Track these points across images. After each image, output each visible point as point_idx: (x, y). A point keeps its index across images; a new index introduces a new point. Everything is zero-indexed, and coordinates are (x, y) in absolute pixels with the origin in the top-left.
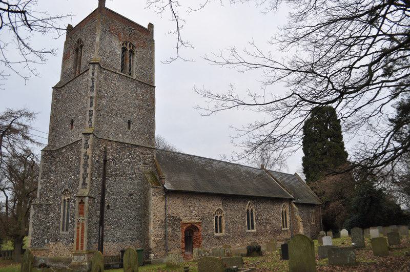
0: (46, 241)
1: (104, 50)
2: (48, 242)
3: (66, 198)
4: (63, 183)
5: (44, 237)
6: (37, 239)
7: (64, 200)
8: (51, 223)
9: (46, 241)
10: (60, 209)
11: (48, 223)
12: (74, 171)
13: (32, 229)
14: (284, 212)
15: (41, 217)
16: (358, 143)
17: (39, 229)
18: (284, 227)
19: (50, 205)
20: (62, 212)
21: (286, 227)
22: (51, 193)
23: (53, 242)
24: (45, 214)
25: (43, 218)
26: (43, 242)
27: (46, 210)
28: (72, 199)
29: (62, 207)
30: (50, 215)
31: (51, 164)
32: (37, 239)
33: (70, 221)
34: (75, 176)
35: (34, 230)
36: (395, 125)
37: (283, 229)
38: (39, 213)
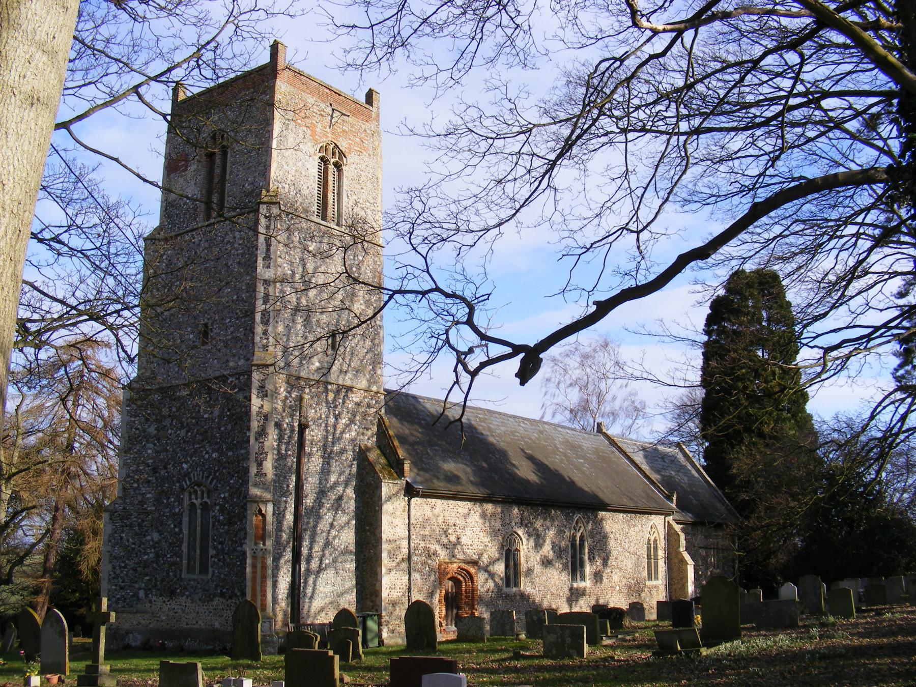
0: (142, 594)
1: (285, 167)
2: (147, 595)
3: (197, 502)
4: (185, 466)
5: (137, 586)
6: (122, 588)
7: (192, 505)
8: (151, 555)
9: (142, 594)
10: (180, 523)
11: (146, 554)
12: (217, 443)
13: (110, 567)
14: (652, 542)
15: (128, 541)
16: (844, 397)
17: (124, 567)
18: (650, 578)
19: (148, 514)
20: (186, 532)
21: (656, 578)
22: (148, 486)
23: (161, 595)
24: (136, 534)
25: (134, 544)
26: (136, 595)
27: (140, 525)
28: (216, 504)
29: (185, 519)
30: (149, 538)
31: (147, 420)
32: (122, 588)
33: (212, 552)
34: (221, 453)
35: (114, 568)
36: (230, 629)
37: (648, 583)
38: (123, 531)
